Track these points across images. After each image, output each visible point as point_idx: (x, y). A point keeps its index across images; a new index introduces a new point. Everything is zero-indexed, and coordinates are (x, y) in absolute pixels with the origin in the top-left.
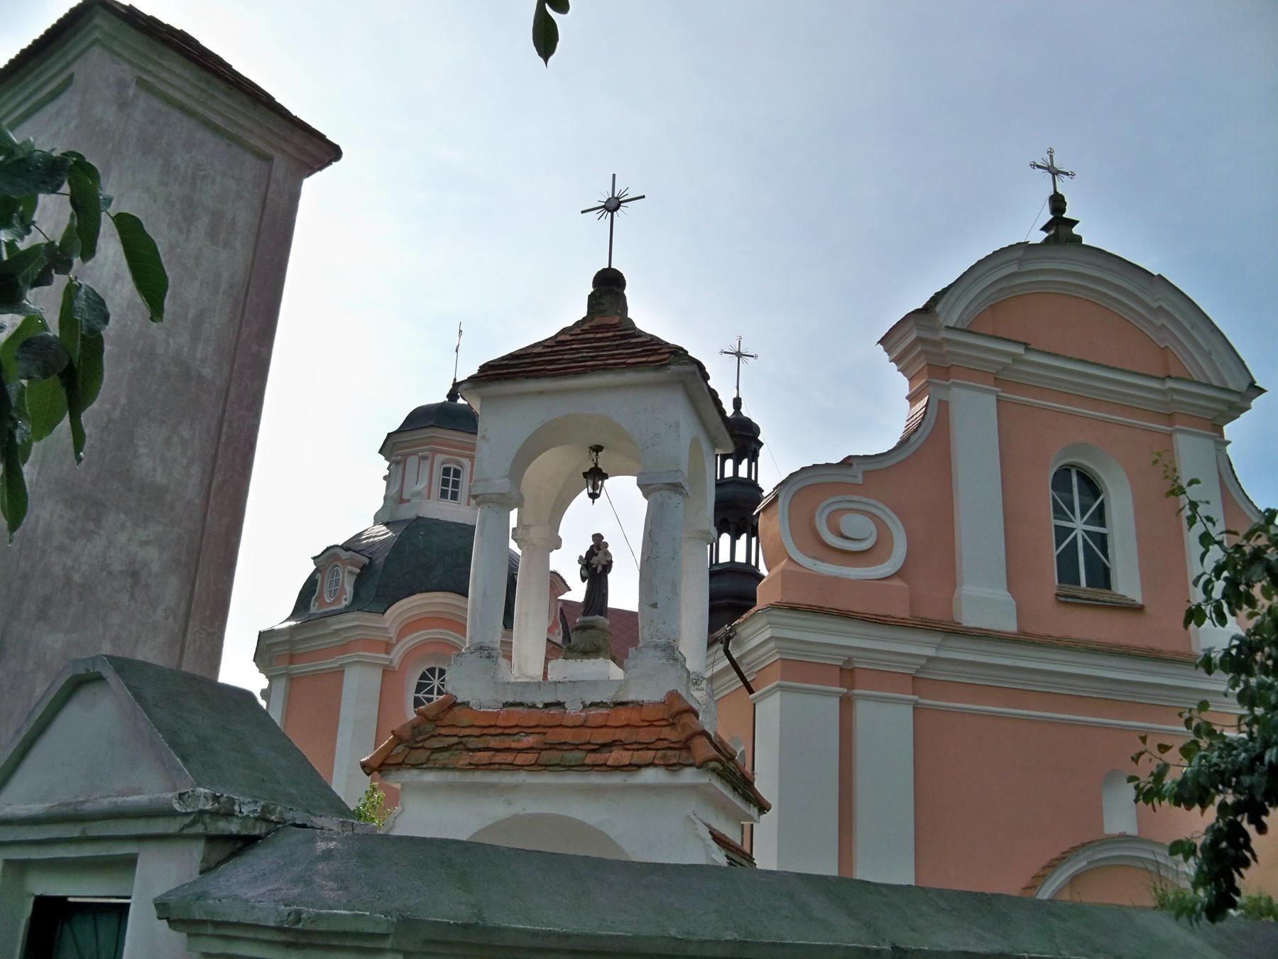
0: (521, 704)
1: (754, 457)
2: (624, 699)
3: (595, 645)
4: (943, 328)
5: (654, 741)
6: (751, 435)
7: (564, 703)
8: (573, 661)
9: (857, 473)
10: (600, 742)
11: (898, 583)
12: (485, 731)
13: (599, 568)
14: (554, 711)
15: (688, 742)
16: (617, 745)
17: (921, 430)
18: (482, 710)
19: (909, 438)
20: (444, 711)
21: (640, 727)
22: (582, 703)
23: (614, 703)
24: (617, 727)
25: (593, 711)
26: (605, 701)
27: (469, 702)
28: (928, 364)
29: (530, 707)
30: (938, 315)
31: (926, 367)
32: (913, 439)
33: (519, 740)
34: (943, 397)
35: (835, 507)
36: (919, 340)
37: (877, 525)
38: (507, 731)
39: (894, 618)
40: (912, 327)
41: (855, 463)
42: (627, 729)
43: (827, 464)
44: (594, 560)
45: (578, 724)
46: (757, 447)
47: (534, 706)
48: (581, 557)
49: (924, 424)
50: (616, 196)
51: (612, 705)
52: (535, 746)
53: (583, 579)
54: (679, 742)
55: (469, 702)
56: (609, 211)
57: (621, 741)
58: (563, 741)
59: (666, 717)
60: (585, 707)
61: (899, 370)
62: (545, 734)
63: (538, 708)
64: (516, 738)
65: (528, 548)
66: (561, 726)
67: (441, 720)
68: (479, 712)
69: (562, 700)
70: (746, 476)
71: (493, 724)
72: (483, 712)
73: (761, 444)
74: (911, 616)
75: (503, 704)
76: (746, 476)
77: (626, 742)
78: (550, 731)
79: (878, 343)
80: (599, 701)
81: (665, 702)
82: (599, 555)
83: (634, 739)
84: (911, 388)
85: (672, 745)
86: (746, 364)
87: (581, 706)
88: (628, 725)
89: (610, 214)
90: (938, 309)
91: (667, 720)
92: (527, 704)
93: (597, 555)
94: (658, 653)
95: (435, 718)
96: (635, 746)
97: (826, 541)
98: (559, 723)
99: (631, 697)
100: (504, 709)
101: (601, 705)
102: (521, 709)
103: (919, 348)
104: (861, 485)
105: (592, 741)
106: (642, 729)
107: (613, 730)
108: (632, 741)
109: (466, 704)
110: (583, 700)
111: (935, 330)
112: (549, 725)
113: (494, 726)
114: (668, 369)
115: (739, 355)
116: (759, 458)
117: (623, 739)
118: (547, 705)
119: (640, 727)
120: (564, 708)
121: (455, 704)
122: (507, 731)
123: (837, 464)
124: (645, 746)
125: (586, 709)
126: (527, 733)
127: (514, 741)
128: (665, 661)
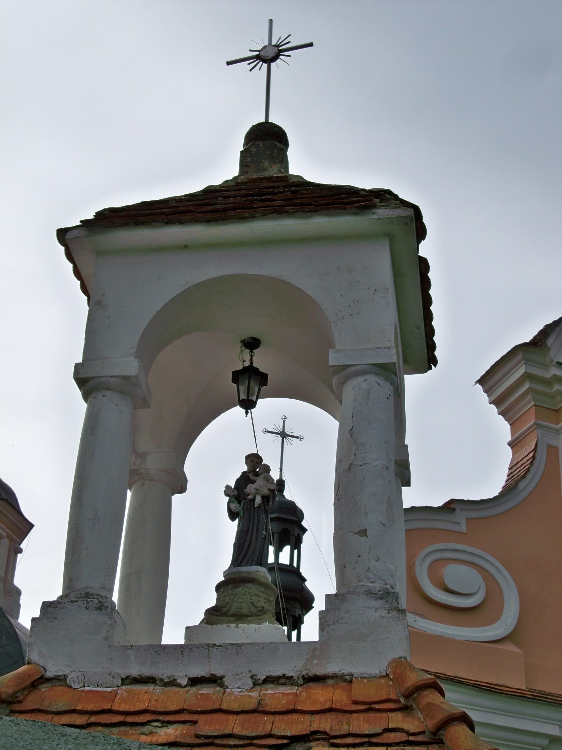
0: (151, 680)
1: (296, 544)
2: (320, 671)
3: (255, 607)
4: (554, 363)
5: (380, 731)
6: (294, 518)
7: (222, 678)
8: (224, 626)
9: (461, 517)
10: (289, 733)
11: (510, 647)
12: (93, 719)
13: (256, 501)
14: (205, 690)
15: (441, 732)
16: (318, 740)
17: (529, 477)
18: (87, 688)
19: (517, 484)
20: (24, 689)
21: (351, 712)
22: (252, 677)
23: (304, 678)
24: (313, 713)
25: (270, 690)
26: (289, 674)
27: (65, 677)
28: (535, 405)
29: (166, 684)
30: (549, 349)
31: (534, 408)
32: (522, 485)
33: (151, 733)
34: (554, 443)
35: (438, 556)
36: (527, 376)
37: (485, 579)
38: (129, 719)
39: (509, 687)
40: (520, 362)
41: (458, 507)
42: (330, 716)
43: (427, 507)
44: (250, 489)
45: (247, 708)
46: (301, 533)
47: (173, 683)
48: (228, 487)
49: (533, 470)
50: (274, 43)
51: (301, 681)
52: (179, 740)
53: (233, 515)
54: (423, 733)
55: (65, 677)
56: (264, 61)
57: (325, 733)
58: (227, 732)
59: (393, 696)
60: (255, 684)
61: (499, 414)
62: (195, 722)
63: (179, 686)
64: (146, 729)
65: (143, 485)
66: (220, 711)
67: (20, 702)
68: (83, 691)
69: (219, 672)
70: (287, 562)
71: (107, 707)
72: (88, 691)
73: (304, 530)
74: (527, 688)
75: (122, 679)
76: (287, 562)
77: (333, 733)
78: (201, 718)
79: (476, 382)
80: (281, 674)
81: (387, 675)
82: (257, 482)
83: (345, 729)
84: (513, 433)
85: (411, 738)
86: (291, 446)
87: (251, 683)
88: (331, 710)
89: (265, 65)
90: (550, 342)
91: (397, 701)
92: (162, 680)
93: (253, 482)
94: (373, 603)
95: (10, 699)
96: (349, 740)
97: (427, 594)
98: (216, 707)
99: (332, 668)
100: (124, 687)
101: (282, 681)
102: (150, 687)
103: (527, 386)
104: (464, 533)
105: (276, 732)
106: (355, 715)
107: (307, 717)
108: (342, 733)
109: (61, 680)
110: (253, 673)
111: (545, 366)
112: (194, 708)
113: (110, 711)
114: (374, 213)
115: (283, 435)
116: (302, 545)
117: (328, 729)
118: (194, 682)
119: (351, 712)
120: (222, 685)
121: (43, 680)
122: (129, 719)
123: (439, 508)
124: (366, 740)
125: (258, 688)
126: (163, 722)
127: (143, 734)
128: (384, 613)
